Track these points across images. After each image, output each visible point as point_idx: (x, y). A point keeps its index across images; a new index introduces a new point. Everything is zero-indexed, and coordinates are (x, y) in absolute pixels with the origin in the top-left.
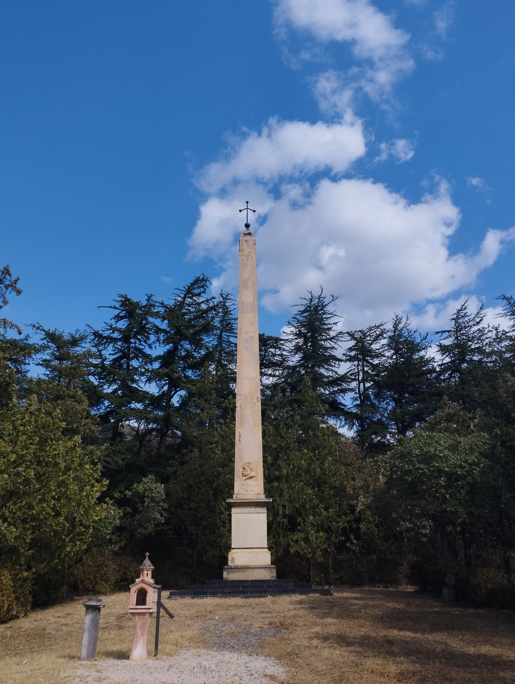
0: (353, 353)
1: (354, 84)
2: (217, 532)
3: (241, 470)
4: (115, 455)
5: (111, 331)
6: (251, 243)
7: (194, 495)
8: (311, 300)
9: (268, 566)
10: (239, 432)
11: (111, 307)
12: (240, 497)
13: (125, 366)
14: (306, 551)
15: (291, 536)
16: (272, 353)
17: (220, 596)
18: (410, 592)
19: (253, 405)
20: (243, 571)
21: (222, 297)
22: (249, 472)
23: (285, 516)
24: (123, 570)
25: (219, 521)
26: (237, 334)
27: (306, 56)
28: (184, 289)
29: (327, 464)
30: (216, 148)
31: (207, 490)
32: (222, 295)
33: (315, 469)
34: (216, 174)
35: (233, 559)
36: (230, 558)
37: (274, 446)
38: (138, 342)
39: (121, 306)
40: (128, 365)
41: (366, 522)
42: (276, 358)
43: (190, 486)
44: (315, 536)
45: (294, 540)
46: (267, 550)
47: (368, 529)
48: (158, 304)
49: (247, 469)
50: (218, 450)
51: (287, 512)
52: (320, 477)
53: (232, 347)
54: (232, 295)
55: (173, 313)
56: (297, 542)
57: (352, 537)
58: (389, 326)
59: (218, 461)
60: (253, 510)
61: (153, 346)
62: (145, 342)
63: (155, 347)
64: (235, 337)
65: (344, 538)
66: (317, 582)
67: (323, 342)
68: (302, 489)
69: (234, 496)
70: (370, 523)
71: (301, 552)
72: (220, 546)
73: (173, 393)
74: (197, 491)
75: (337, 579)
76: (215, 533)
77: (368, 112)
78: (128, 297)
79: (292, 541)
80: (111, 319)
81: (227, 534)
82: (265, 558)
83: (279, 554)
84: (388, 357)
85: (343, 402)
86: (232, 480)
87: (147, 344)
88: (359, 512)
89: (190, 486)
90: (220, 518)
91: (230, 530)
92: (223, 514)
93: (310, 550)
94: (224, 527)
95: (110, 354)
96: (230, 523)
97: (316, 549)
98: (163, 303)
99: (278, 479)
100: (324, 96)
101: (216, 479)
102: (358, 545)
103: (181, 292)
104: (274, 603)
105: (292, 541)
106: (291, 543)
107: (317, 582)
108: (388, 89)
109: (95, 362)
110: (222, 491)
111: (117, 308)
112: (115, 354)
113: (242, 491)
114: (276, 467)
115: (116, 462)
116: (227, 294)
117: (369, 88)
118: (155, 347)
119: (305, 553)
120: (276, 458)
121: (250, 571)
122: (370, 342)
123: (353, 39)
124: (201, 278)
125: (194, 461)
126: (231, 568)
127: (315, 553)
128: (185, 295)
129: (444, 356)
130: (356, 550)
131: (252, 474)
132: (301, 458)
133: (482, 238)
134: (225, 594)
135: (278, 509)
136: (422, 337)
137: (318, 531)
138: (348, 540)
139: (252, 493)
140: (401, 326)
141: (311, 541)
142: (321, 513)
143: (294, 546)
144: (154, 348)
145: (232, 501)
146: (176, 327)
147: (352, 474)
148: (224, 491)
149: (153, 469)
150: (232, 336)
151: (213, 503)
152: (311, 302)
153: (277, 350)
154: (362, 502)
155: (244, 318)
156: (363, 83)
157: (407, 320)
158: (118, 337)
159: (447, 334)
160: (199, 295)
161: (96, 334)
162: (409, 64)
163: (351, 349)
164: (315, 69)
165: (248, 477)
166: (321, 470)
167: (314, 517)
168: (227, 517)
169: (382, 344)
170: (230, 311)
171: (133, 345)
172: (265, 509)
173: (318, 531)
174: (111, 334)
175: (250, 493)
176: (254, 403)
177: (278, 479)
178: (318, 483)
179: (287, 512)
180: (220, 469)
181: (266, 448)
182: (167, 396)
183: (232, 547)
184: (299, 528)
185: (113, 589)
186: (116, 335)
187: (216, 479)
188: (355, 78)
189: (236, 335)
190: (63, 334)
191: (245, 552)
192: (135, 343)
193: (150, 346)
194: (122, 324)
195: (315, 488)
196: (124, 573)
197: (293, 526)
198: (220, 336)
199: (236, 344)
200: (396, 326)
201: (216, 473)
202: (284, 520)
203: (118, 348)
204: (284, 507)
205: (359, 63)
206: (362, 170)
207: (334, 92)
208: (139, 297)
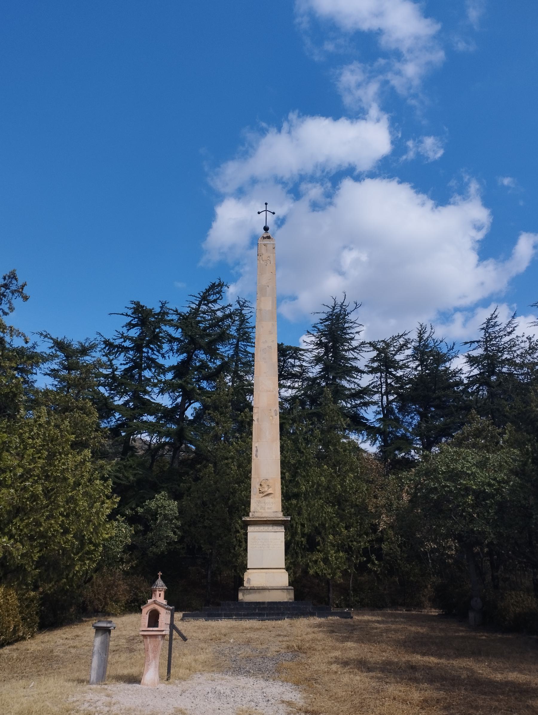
0: (375, 365)
1: (381, 77)
2: (233, 551)
3: (258, 486)
4: (126, 470)
6: (270, 247)
7: (208, 513)
9: (286, 588)
10: (256, 447)
11: (122, 314)
12: (257, 515)
14: (325, 572)
16: (291, 363)
17: (235, 618)
19: (271, 418)
20: (259, 592)
21: (239, 304)
22: (266, 489)
23: (303, 535)
24: (133, 591)
25: (234, 539)
26: (254, 343)
27: (329, 47)
29: (347, 481)
30: (233, 145)
32: (239, 303)
33: (335, 485)
34: (233, 172)
35: (249, 580)
36: (245, 579)
37: (293, 462)
38: (150, 351)
40: (140, 376)
41: (388, 542)
42: (295, 369)
43: (204, 504)
44: (335, 557)
46: (284, 570)
47: (391, 549)
48: (172, 312)
49: (265, 486)
50: (234, 465)
51: (306, 530)
52: (340, 494)
53: (249, 357)
55: (187, 321)
56: (316, 562)
57: (374, 557)
60: (270, 528)
61: (166, 356)
62: (158, 351)
63: (169, 356)
64: (252, 346)
65: (365, 559)
66: (337, 604)
68: (322, 506)
69: (250, 514)
72: (236, 566)
73: (186, 405)
74: (211, 508)
75: (358, 602)
76: (230, 552)
77: (394, 107)
79: (310, 561)
80: (123, 327)
82: (282, 578)
83: (297, 575)
84: (412, 369)
85: (366, 416)
86: (249, 497)
87: (160, 353)
88: (381, 532)
89: (204, 504)
90: (236, 537)
91: (246, 550)
92: (239, 532)
93: (330, 571)
94: (240, 546)
95: (121, 364)
96: (246, 542)
97: (335, 569)
98: (177, 311)
99: (296, 496)
101: (231, 496)
102: (379, 566)
103: (195, 298)
104: (291, 625)
106: (310, 564)
107: (337, 604)
108: (416, 82)
109: (105, 372)
111: (129, 316)
112: (127, 363)
113: (259, 508)
115: (127, 478)
116: (244, 301)
117: (396, 82)
118: (169, 356)
119: (325, 574)
120: (295, 474)
121: (267, 593)
122: (393, 352)
124: (217, 283)
126: (247, 589)
127: (334, 574)
129: (473, 368)
130: (377, 571)
131: (270, 491)
132: (321, 475)
135: (296, 528)
136: (449, 348)
137: (337, 551)
138: (369, 560)
139: (269, 511)
140: (426, 336)
141: (331, 562)
143: (312, 566)
144: (167, 358)
145: (248, 519)
147: (375, 492)
148: (240, 508)
149: (166, 485)
150: (249, 346)
151: (228, 520)
152: (333, 310)
153: (296, 361)
154: (384, 522)
155: (263, 327)
156: (390, 76)
157: (432, 329)
158: (130, 346)
159: (476, 344)
160: (215, 301)
161: (107, 343)
163: (373, 360)
164: (339, 61)
165: (265, 494)
166: (342, 487)
168: (243, 536)
170: (247, 319)
171: (146, 354)
173: (337, 551)
175: (267, 510)
176: (272, 416)
177: (296, 496)
178: (339, 501)
179: (306, 532)
180: (236, 485)
181: (284, 464)
182: (181, 408)
186: (127, 344)
187: (231, 496)
188: (382, 71)
190: (72, 343)
191: (261, 573)
192: (148, 352)
193: (163, 356)
194: (134, 333)
195: (335, 506)
196: (136, 594)
197: (312, 545)
198: (237, 346)
199: (253, 354)
200: (420, 335)
201: (231, 490)
203: (129, 358)
205: (385, 55)
206: (387, 169)
207: (359, 85)
208: (152, 304)
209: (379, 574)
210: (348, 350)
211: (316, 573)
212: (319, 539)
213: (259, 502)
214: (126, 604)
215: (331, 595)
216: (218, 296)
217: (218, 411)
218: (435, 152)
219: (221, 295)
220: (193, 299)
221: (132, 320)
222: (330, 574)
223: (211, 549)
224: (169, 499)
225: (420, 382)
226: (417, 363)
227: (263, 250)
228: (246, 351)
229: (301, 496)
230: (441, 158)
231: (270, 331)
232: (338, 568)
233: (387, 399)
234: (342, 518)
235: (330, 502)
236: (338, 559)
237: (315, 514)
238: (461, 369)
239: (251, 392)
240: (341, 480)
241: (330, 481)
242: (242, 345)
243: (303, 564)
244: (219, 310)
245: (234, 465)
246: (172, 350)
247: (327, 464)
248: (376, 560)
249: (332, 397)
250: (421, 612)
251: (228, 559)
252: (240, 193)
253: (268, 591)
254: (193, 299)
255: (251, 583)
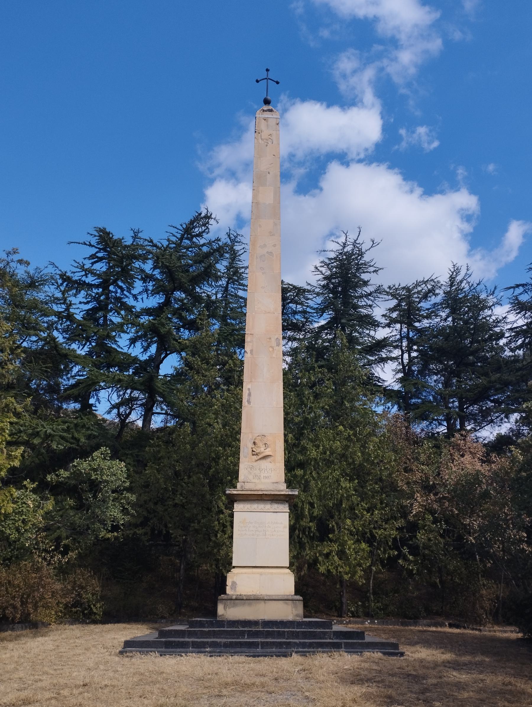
0: (394, 315)
1: (378, 64)
2: (213, 539)
3: (250, 445)
4: (77, 431)
5: (84, 273)
7: (182, 486)
8: (344, 245)
9: (290, 598)
11: (85, 244)
12: (248, 486)
13: (101, 321)
14: (341, 570)
15: (319, 548)
16: (292, 309)
18: (508, 641)
19: (271, 349)
20: (250, 605)
21: (230, 238)
22: (262, 449)
23: (312, 518)
24: (76, 591)
25: (216, 523)
27: (325, 33)
28: (182, 229)
29: (371, 447)
30: (228, 131)
31: (199, 478)
32: (229, 236)
33: (355, 453)
34: (225, 155)
35: (234, 584)
36: (229, 582)
37: (297, 420)
38: (119, 291)
39: (98, 243)
41: (425, 530)
42: (297, 317)
43: (177, 474)
44: (354, 549)
45: (324, 554)
46: (288, 571)
47: (429, 540)
50: (217, 422)
51: (316, 512)
52: (360, 465)
54: (242, 236)
56: (327, 556)
57: (406, 550)
58: (444, 279)
59: (216, 437)
60: (268, 506)
61: (139, 297)
62: (129, 291)
64: (244, 290)
65: (396, 553)
66: (352, 613)
67: (355, 301)
68: (338, 480)
69: (239, 485)
70: (431, 531)
71: (334, 572)
72: (217, 560)
73: (163, 356)
75: (381, 610)
76: (210, 540)
77: (389, 97)
78: (108, 230)
79: (320, 555)
80: (85, 259)
81: (228, 543)
82: (285, 583)
83: (302, 573)
85: (382, 376)
86: (237, 464)
87: (130, 293)
88: (414, 516)
90: (218, 520)
91: (231, 537)
92: (223, 513)
93: (348, 569)
94: (224, 532)
96: (232, 527)
97: (355, 567)
98: (151, 241)
99: (301, 465)
100: (344, 76)
101: (213, 464)
102: (415, 563)
103: (177, 230)
104: (307, 674)
105: (320, 555)
106: (320, 558)
107: (352, 613)
108: (412, 71)
110: (222, 480)
111: (93, 246)
112: (88, 303)
113: (251, 477)
114: (299, 449)
115: (78, 440)
116: (235, 234)
117: (392, 69)
119: (340, 572)
120: (299, 436)
121: (261, 605)
123: (375, 16)
124: (203, 215)
125: (184, 438)
126: (231, 599)
127: (354, 573)
128: (183, 236)
130: (412, 570)
131: (268, 452)
132: (330, 440)
133: (505, 230)
134: (218, 649)
135: (303, 509)
136: (489, 292)
138: (401, 555)
140: (459, 278)
141: (349, 558)
142: (363, 516)
144: (140, 300)
145: (235, 492)
146: (167, 267)
147: (406, 463)
148: (224, 480)
149: (130, 452)
150: (241, 289)
152: (344, 247)
153: (299, 306)
155: (260, 226)
156: (385, 62)
157: (468, 270)
158: (93, 283)
159: (521, 289)
160: (200, 235)
161: (64, 277)
162: (436, 45)
163: (392, 310)
164: (334, 48)
165: (261, 456)
166: (363, 453)
167: (353, 522)
168: (228, 519)
169: (432, 302)
171: (113, 294)
172: (287, 505)
173: (358, 541)
174: (82, 276)
176: (272, 347)
177: (301, 465)
178: (359, 474)
179: (315, 514)
180: (220, 448)
181: (287, 422)
182: (156, 362)
183: (234, 564)
184: (331, 536)
185: (62, 617)
186: (90, 279)
187: (213, 464)
188: (379, 56)
189: (246, 288)
192: (116, 292)
193: (135, 297)
194: (101, 267)
195: (354, 480)
196: (79, 595)
197: (324, 532)
198: (226, 289)
199: (245, 300)
200: (452, 279)
201: (213, 455)
202: (311, 524)
203: (91, 295)
204: (312, 505)
205: (381, 41)
206: (382, 155)
207: (354, 72)
208: (122, 233)
209: (415, 574)
210: (361, 297)
211: (329, 571)
212: (332, 524)
213: (252, 468)
214: (65, 609)
215: (344, 600)
216: (203, 228)
217: (199, 356)
218: (430, 143)
219: (207, 227)
220: (174, 231)
221: (97, 252)
222: (347, 574)
223: (185, 535)
224: (112, 458)
225: (452, 335)
226: (447, 311)
227: (263, 125)
228: (236, 296)
229: (310, 464)
230: (435, 149)
231: (270, 232)
232: (360, 565)
233: (409, 356)
234: (363, 497)
235: (347, 475)
236: (358, 552)
237: (328, 490)
238: (505, 318)
239: (241, 344)
240: (362, 446)
241: (346, 447)
242: (233, 288)
243: (310, 558)
244: (204, 245)
245: (217, 422)
246: (146, 290)
247: (342, 424)
248: (410, 553)
249: (347, 342)
250: (480, 630)
251: (206, 549)
252: (232, 176)
253: (262, 602)
254: (174, 231)
255: (237, 589)
